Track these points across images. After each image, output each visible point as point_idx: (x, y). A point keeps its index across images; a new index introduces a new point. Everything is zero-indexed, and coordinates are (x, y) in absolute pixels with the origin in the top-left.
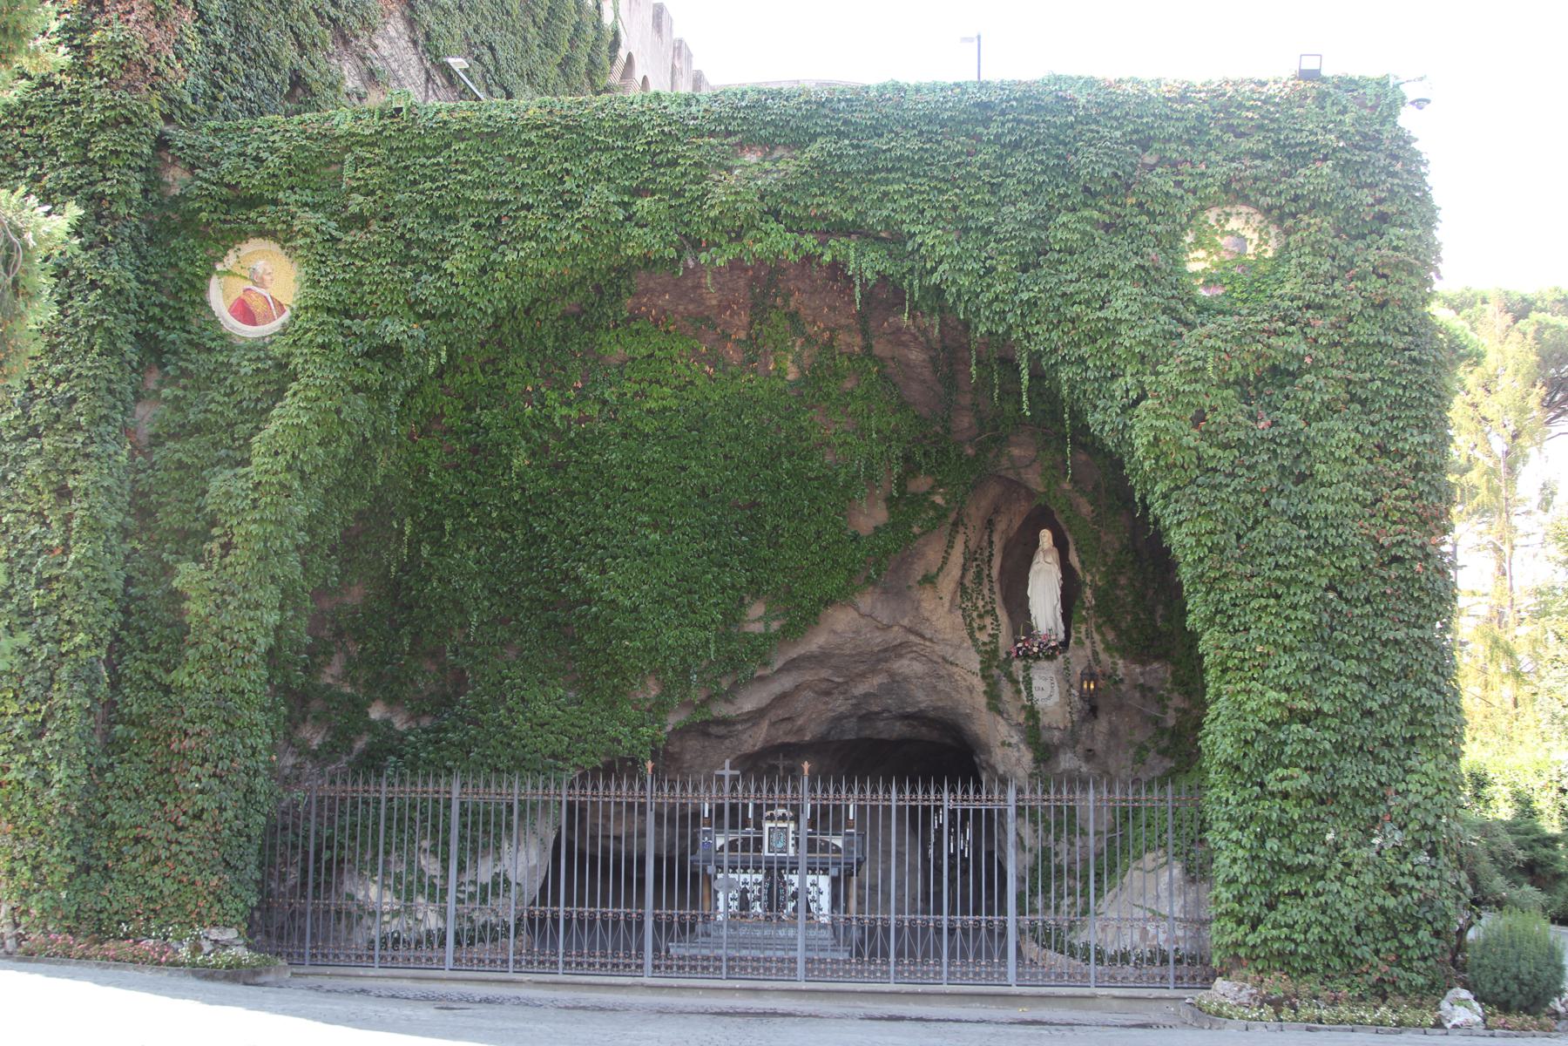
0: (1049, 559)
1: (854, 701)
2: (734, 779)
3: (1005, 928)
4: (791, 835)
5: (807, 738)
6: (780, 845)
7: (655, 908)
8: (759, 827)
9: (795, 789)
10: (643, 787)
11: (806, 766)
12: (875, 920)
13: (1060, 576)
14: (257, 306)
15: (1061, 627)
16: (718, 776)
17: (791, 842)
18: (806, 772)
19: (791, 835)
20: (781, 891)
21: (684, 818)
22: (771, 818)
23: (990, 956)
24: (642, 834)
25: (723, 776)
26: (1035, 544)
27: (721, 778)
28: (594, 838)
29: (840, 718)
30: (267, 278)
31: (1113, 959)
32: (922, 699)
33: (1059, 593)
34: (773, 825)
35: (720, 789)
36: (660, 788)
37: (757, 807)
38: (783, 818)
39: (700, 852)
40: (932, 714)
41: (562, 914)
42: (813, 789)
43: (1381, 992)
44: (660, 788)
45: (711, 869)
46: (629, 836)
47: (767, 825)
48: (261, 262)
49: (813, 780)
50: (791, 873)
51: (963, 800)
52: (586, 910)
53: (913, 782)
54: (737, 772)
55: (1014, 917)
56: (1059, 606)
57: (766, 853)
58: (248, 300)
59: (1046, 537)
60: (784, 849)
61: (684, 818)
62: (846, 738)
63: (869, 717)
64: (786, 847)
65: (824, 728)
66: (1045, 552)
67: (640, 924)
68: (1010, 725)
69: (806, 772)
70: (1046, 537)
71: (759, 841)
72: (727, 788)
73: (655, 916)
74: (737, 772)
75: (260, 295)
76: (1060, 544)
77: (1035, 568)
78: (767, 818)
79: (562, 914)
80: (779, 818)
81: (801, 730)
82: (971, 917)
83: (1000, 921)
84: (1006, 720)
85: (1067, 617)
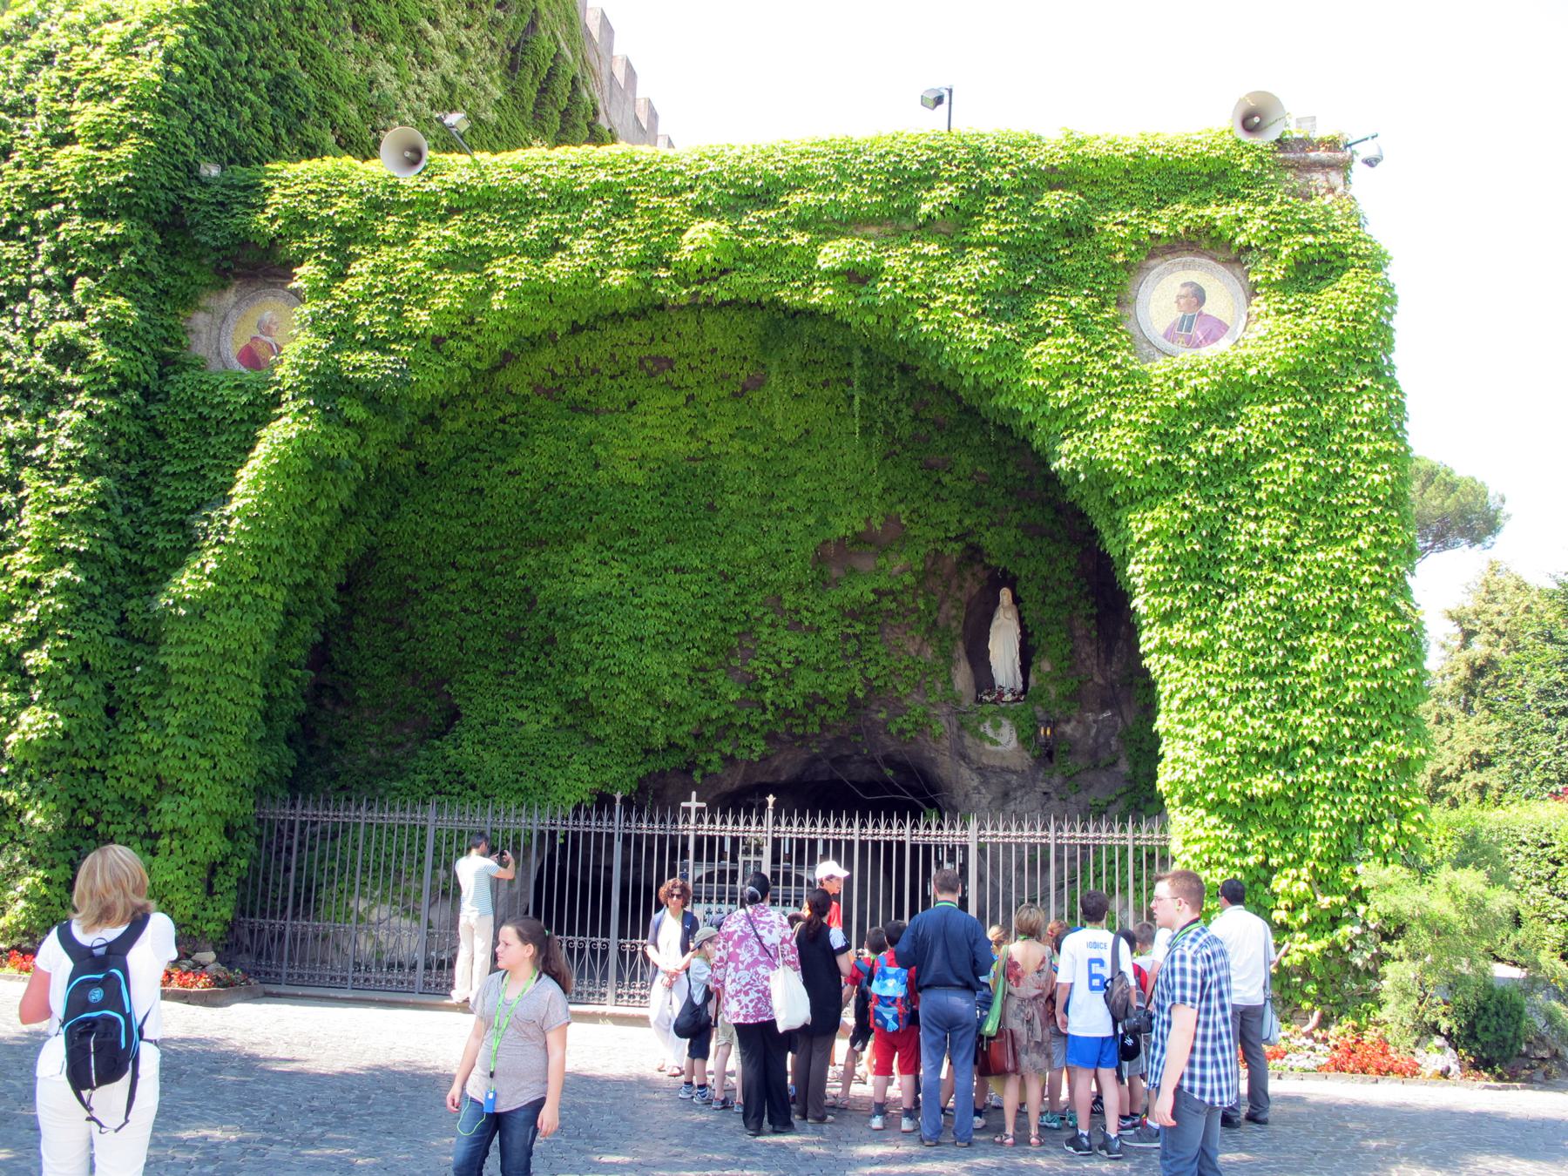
0: (1009, 615)
2: (700, 811)
8: (734, 859)
9: (760, 822)
10: (611, 818)
11: (771, 799)
15: (1019, 678)
18: (770, 807)
23: (592, 976)
26: (997, 602)
29: (815, 759)
31: (391, 966)
35: (686, 820)
36: (628, 819)
40: (898, 758)
42: (777, 822)
43: (1418, 644)
44: (628, 819)
49: (777, 813)
53: (864, 816)
54: (704, 805)
59: (1005, 595)
62: (820, 779)
63: (839, 761)
67: (605, 953)
69: (770, 807)
70: (1005, 595)
71: (734, 873)
72: (693, 819)
74: (704, 805)
76: (1017, 600)
77: (995, 623)
81: (777, 770)
85: (1025, 668)
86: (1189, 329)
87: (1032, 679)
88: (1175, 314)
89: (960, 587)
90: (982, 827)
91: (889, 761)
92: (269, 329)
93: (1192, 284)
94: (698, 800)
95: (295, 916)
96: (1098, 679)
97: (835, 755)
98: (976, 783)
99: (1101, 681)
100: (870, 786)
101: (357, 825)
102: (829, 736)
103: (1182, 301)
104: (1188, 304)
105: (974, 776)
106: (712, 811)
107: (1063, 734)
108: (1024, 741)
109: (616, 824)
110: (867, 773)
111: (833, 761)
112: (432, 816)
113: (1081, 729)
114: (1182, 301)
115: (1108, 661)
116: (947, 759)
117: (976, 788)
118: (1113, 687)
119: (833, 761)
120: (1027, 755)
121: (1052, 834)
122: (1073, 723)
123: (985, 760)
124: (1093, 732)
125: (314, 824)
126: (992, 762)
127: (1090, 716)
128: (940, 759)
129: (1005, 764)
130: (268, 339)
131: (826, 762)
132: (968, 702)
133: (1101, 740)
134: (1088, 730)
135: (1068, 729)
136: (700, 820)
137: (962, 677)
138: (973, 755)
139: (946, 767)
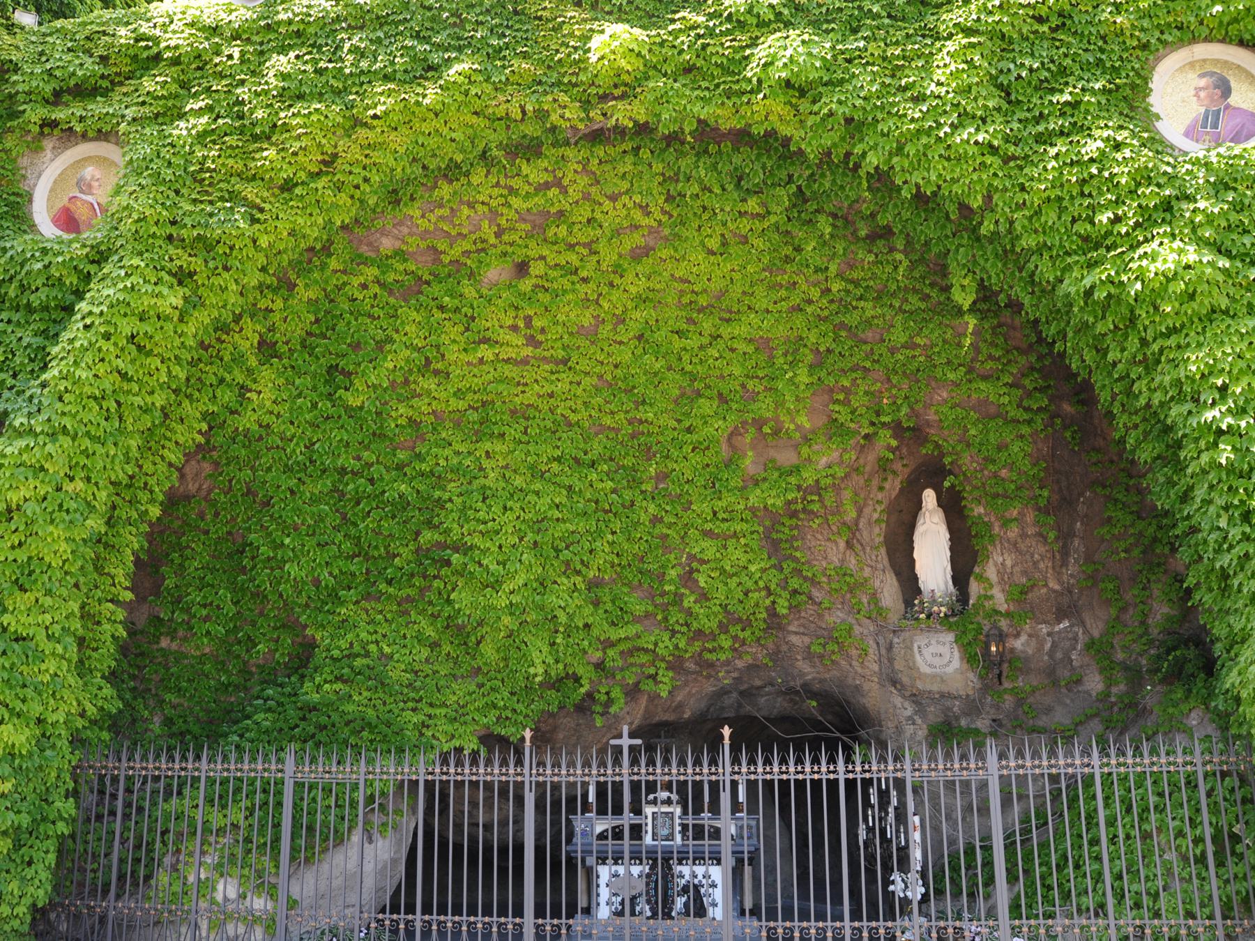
1: (735, 675)
3: (521, 933)
4: (677, 821)
5: (686, 716)
6: (666, 832)
7: (536, 917)
8: (637, 811)
10: (519, 762)
11: (726, 731)
12: (559, 927)
13: (948, 536)
14: (81, 213)
16: (613, 746)
17: (678, 828)
18: (727, 741)
19: (677, 821)
20: (653, 892)
21: (556, 804)
22: (654, 802)
24: (519, 821)
25: (621, 747)
26: (919, 505)
27: (618, 750)
28: (458, 827)
29: (724, 692)
30: (96, 184)
32: (807, 671)
33: (949, 554)
34: (656, 810)
36: (541, 764)
37: (635, 786)
38: (668, 802)
39: (578, 840)
41: (418, 925)
42: (736, 761)
45: (591, 861)
46: (503, 823)
47: (649, 810)
48: (90, 169)
49: (735, 749)
50: (680, 863)
51: (962, 769)
52: (418, 918)
54: (639, 742)
55: (1008, 922)
56: (949, 568)
57: (648, 839)
58: (73, 208)
59: (929, 497)
60: (670, 837)
61: (556, 804)
64: (672, 834)
65: (703, 705)
66: (931, 512)
68: (904, 697)
69: (727, 741)
70: (929, 497)
73: (537, 927)
74: (639, 742)
75: (86, 202)
78: (648, 803)
79: (418, 925)
80: (663, 802)
81: (680, 706)
82: (813, 923)
83: (818, 929)
84: (899, 690)
86: (1215, 126)
87: (974, 588)
88: (1196, 110)
89: (881, 488)
90: (1002, 756)
91: (809, 691)
92: (90, 186)
93: (1212, 74)
94: (620, 736)
95: (118, 897)
96: (1054, 585)
97: (744, 687)
98: (909, 712)
99: (1057, 587)
100: (783, 720)
101: (196, 780)
102: (740, 664)
103: (1202, 94)
104: (1210, 97)
105: (907, 704)
106: (650, 749)
107: (1012, 650)
108: (969, 659)
109: (526, 771)
110: (780, 705)
111: (741, 693)
112: (290, 765)
113: (1034, 642)
114: (1202, 94)
115: (1064, 563)
116: (875, 686)
117: (909, 718)
118: (1070, 592)
119: (741, 693)
120: (971, 675)
121: (204, 764)
122: (1023, 638)
123: (920, 685)
124: (1048, 646)
125: (156, 779)
126: (928, 687)
127: (1044, 629)
128: (866, 686)
129: (945, 689)
130: (90, 198)
131: (735, 695)
132: (894, 618)
133: (1059, 655)
134: (1041, 644)
135: (1018, 644)
136: (634, 762)
137: (889, 591)
138: (905, 680)
139: (874, 696)
